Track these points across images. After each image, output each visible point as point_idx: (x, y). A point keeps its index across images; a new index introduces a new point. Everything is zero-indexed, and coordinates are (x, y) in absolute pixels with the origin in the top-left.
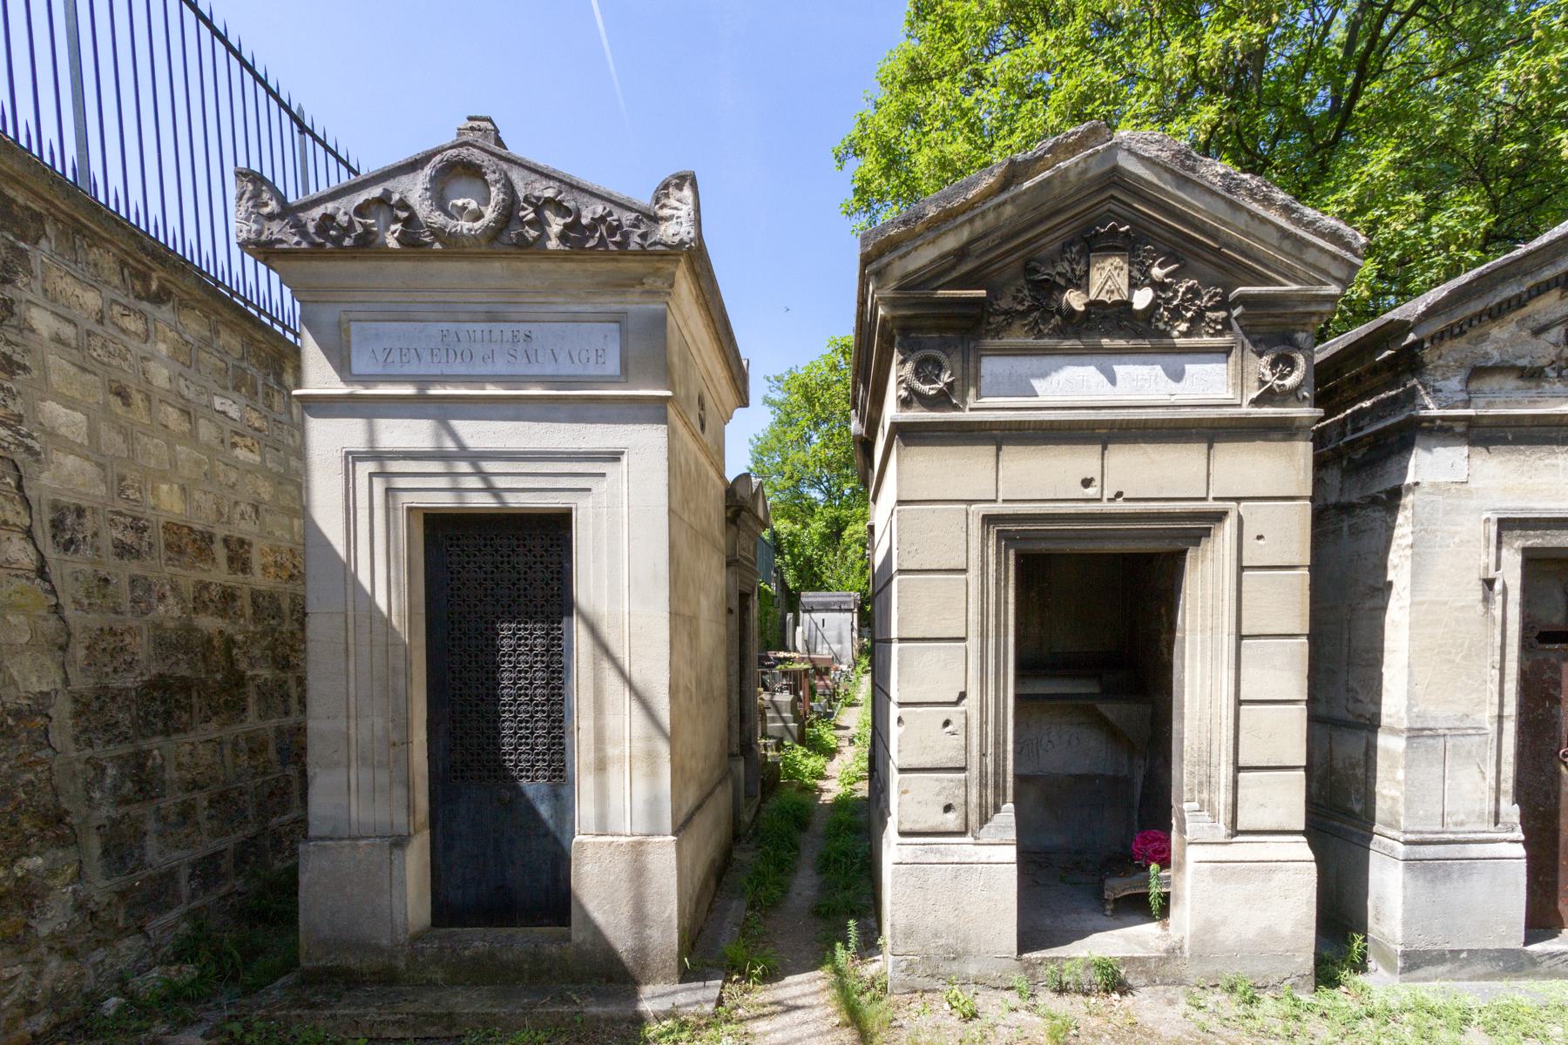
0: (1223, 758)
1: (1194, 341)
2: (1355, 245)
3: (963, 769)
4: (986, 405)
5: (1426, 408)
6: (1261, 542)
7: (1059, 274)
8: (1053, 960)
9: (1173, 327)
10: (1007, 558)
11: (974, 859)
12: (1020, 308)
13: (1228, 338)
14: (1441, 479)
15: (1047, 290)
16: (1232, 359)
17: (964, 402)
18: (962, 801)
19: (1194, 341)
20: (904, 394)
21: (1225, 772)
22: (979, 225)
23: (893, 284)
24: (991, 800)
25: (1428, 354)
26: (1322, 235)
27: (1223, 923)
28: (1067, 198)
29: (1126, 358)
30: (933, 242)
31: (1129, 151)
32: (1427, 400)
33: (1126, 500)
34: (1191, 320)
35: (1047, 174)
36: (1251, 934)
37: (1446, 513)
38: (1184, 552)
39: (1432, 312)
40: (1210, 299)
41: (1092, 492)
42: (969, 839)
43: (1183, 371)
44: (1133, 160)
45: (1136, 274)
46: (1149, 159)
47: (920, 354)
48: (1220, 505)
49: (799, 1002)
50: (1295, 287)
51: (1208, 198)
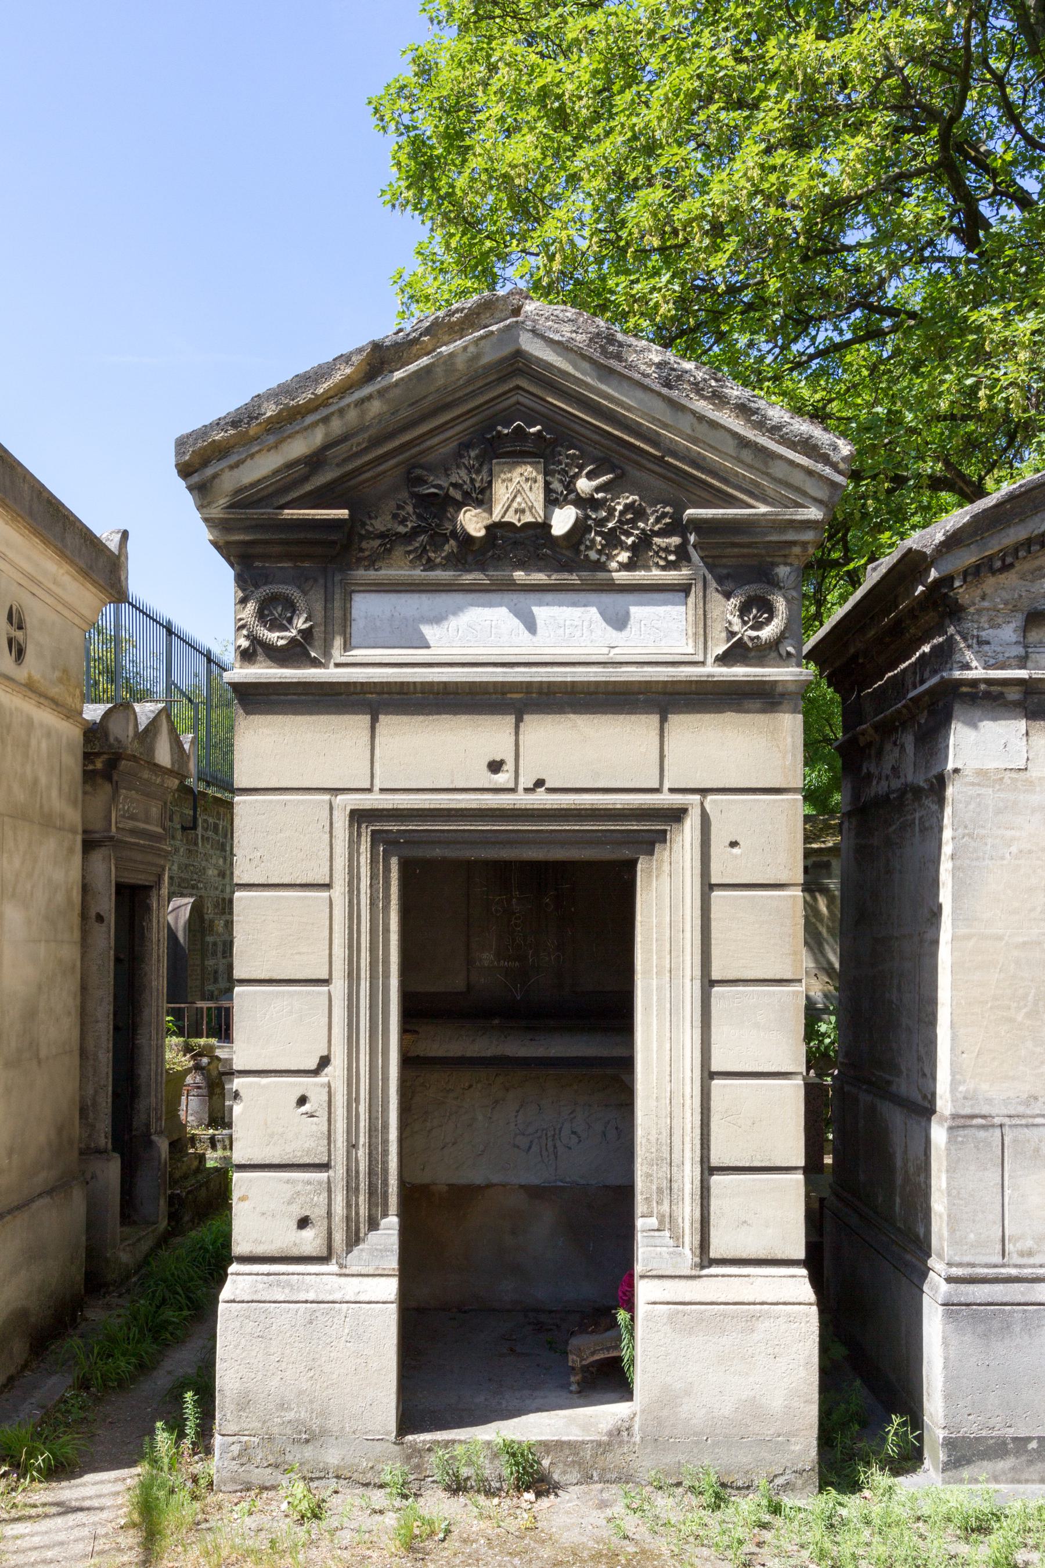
0: (688, 1154)
1: (639, 576)
2: (835, 458)
3: (325, 1167)
4: (358, 661)
5: (967, 667)
6: (736, 851)
7: (455, 485)
8: (447, 1444)
9: (611, 557)
10: (387, 870)
11: (337, 1297)
12: (401, 529)
13: (685, 572)
14: (991, 765)
15: (439, 508)
16: (691, 600)
17: (327, 653)
18: (323, 1212)
19: (639, 576)
20: (245, 643)
21: (689, 1174)
22: (337, 426)
23: (223, 501)
24: (363, 1211)
25: (962, 592)
26: (792, 445)
27: (688, 1393)
28: (454, 391)
29: (549, 597)
30: (276, 446)
31: (534, 331)
32: (969, 656)
33: (550, 790)
34: (634, 548)
35: (425, 361)
36: (726, 1408)
37: (998, 812)
38: (632, 864)
39: (954, 541)
40: (658, 520)
41: (502, 779)
42: (332, 1267)
43: (627, 615)
44: (540, 343)
45: (557, 486)
46: (558, 343)
47: (265, 590)
48: (678, 799)
49: (87, 1504)
50: (763, 509)
51: (640, 394)
